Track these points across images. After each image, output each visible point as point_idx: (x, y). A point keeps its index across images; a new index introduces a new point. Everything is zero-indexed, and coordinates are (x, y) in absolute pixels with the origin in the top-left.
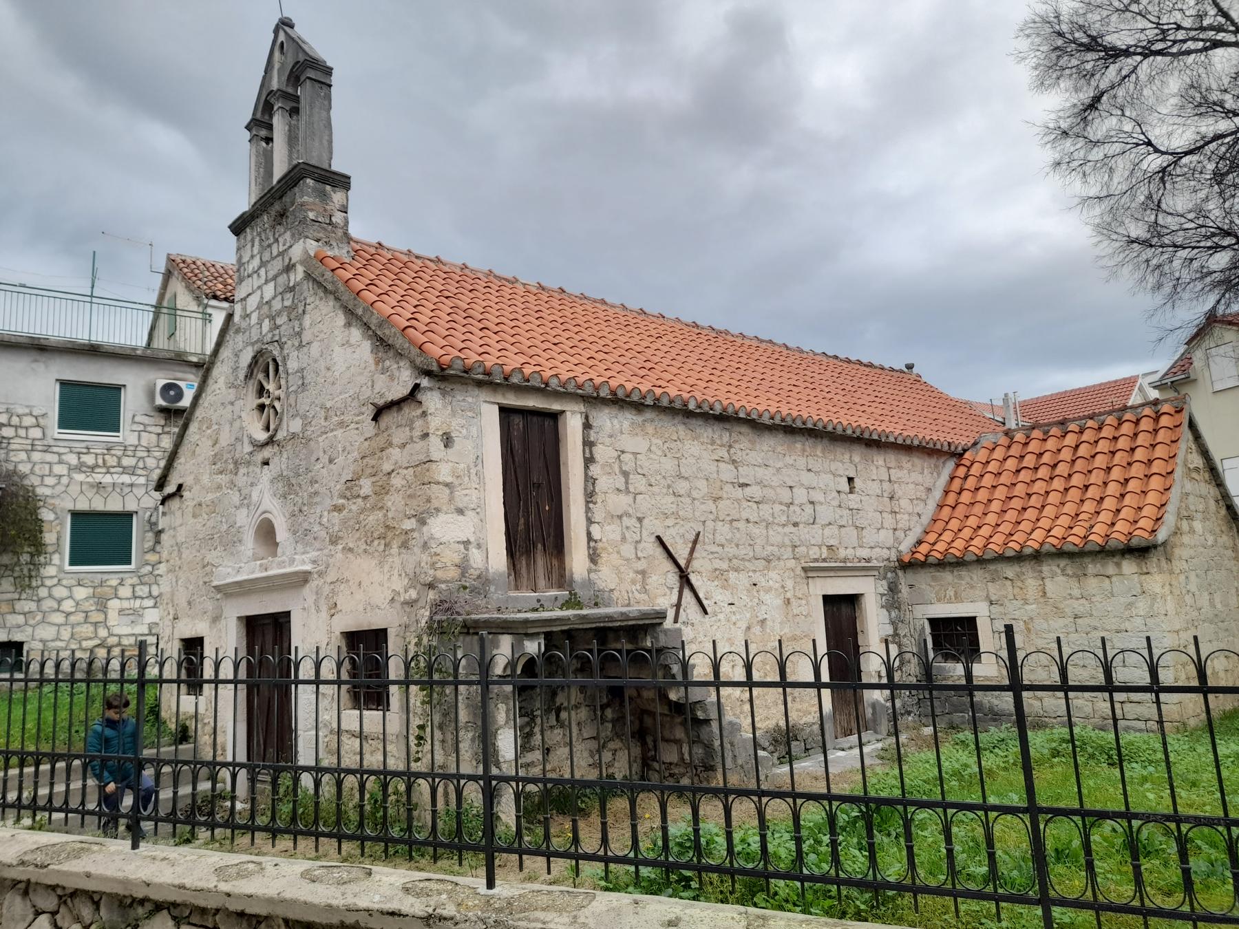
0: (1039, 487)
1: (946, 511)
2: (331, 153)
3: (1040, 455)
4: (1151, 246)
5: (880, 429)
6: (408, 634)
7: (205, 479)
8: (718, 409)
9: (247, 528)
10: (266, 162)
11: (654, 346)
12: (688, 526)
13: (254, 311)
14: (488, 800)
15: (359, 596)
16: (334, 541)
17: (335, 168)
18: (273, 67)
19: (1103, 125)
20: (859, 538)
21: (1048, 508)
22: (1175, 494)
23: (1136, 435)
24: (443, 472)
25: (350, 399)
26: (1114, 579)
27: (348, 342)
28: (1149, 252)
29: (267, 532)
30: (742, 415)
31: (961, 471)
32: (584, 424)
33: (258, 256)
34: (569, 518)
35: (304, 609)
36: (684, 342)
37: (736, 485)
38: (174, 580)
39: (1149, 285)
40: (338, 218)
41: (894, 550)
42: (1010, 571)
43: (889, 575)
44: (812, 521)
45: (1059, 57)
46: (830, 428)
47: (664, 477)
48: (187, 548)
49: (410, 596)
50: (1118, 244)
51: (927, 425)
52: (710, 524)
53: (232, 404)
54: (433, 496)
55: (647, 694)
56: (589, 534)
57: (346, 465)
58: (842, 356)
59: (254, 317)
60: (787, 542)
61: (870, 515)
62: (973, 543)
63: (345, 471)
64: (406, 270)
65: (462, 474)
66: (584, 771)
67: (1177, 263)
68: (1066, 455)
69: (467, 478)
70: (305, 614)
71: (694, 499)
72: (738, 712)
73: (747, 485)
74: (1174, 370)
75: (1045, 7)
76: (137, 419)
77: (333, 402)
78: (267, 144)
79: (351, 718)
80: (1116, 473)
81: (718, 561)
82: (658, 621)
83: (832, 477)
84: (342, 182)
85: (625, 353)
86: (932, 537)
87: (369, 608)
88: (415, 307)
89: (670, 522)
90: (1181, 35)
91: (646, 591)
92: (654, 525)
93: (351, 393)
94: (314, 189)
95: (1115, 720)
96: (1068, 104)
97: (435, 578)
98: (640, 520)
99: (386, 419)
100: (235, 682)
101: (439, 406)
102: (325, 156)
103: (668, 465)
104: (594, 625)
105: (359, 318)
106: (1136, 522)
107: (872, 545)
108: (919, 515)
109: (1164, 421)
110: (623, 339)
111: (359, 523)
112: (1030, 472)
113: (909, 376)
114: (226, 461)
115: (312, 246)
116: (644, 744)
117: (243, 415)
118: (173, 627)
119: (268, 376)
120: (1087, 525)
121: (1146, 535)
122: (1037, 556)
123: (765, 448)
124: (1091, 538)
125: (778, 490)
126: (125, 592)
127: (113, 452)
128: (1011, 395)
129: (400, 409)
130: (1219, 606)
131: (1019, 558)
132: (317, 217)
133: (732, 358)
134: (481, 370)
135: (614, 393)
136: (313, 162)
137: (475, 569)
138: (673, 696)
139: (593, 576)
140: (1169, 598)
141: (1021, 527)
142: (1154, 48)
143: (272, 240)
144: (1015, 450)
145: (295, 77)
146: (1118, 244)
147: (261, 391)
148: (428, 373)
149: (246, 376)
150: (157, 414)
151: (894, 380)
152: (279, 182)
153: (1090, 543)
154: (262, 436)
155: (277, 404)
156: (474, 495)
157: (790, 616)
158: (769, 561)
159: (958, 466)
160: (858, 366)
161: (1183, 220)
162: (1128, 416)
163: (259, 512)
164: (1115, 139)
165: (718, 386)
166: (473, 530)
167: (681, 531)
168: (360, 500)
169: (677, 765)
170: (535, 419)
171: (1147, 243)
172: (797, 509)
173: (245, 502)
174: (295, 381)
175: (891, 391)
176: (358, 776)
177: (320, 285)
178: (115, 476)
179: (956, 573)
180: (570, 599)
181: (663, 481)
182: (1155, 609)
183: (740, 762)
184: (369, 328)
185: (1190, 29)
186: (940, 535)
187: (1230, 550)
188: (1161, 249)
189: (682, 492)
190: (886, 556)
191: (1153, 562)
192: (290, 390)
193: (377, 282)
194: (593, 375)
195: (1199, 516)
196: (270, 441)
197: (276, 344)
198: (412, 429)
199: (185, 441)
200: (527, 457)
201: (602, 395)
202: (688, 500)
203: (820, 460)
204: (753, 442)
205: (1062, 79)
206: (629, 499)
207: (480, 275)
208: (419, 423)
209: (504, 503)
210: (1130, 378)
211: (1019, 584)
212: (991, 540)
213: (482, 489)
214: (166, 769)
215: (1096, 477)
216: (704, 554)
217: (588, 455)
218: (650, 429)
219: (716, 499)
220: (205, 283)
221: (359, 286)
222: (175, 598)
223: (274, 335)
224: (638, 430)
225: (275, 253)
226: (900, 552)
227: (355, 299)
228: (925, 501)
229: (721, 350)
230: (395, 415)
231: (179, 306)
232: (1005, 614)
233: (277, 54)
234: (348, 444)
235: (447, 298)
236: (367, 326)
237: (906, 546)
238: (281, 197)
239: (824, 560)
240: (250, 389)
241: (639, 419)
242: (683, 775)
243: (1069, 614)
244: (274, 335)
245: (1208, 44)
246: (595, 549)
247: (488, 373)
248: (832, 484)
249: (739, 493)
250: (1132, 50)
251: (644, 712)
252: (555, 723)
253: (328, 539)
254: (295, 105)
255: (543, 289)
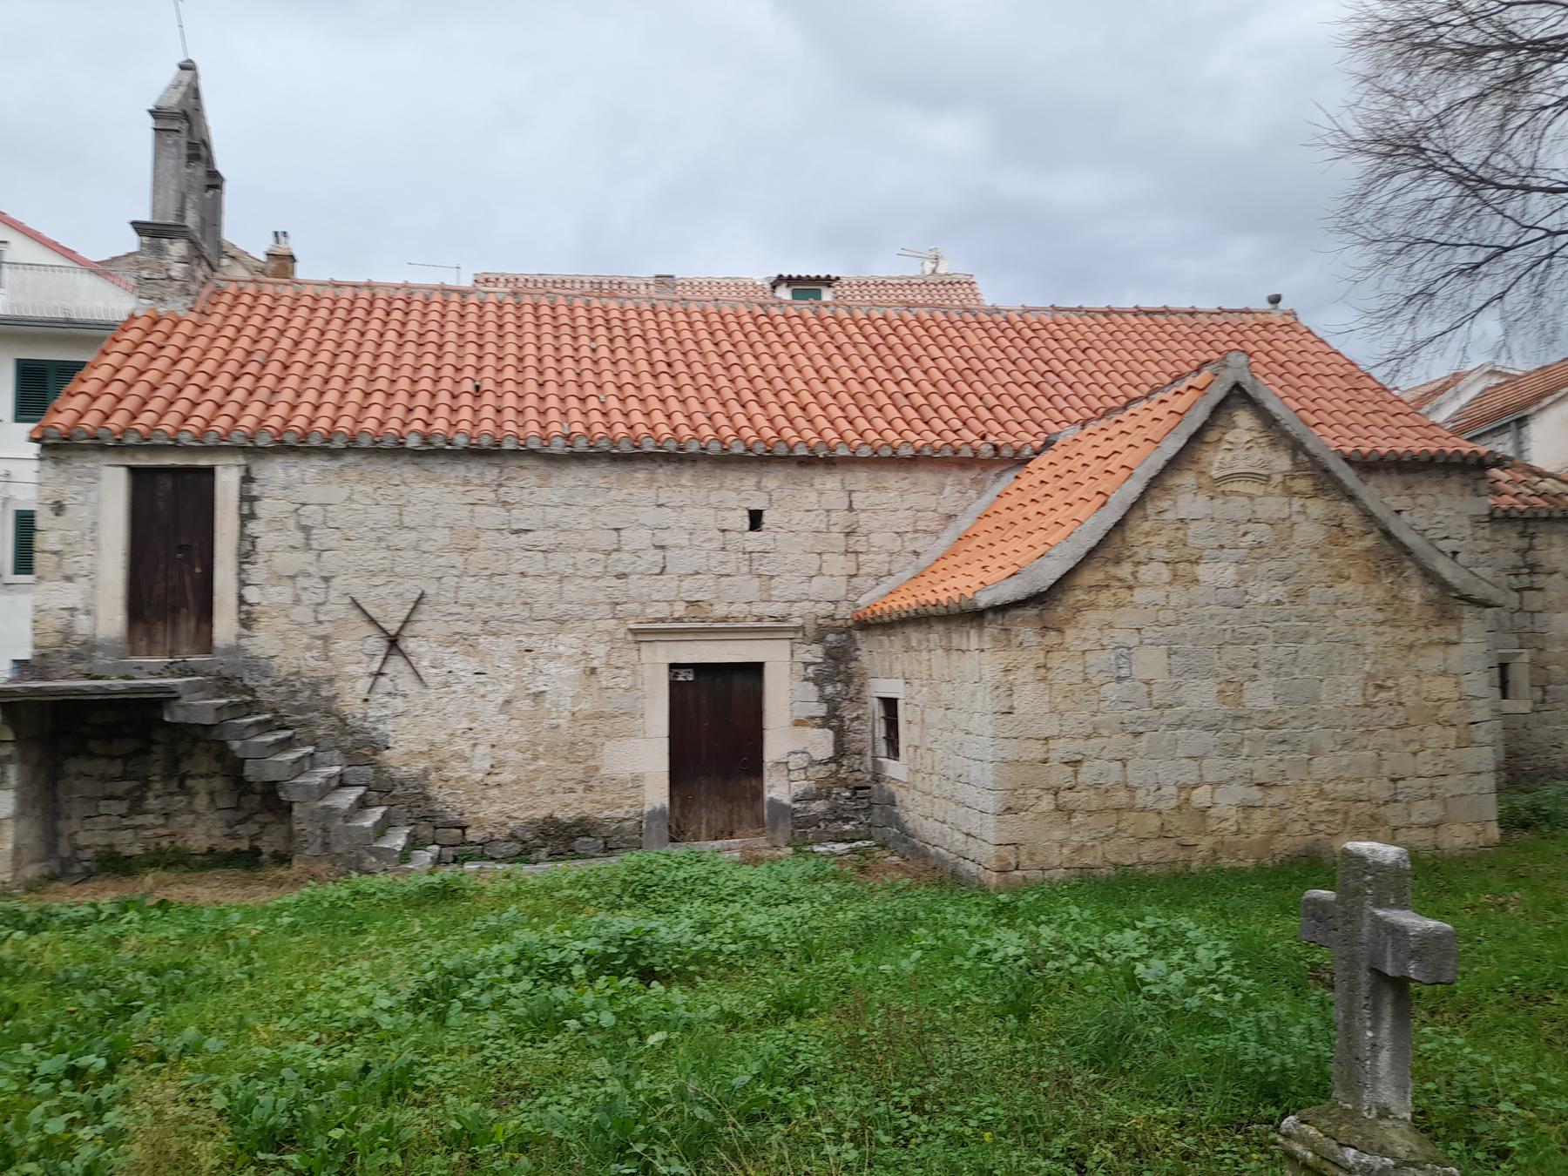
12: (409, 584)
103: (383, 515)
139: (244, 642)
218: (352, 475)
246: (248, 613)
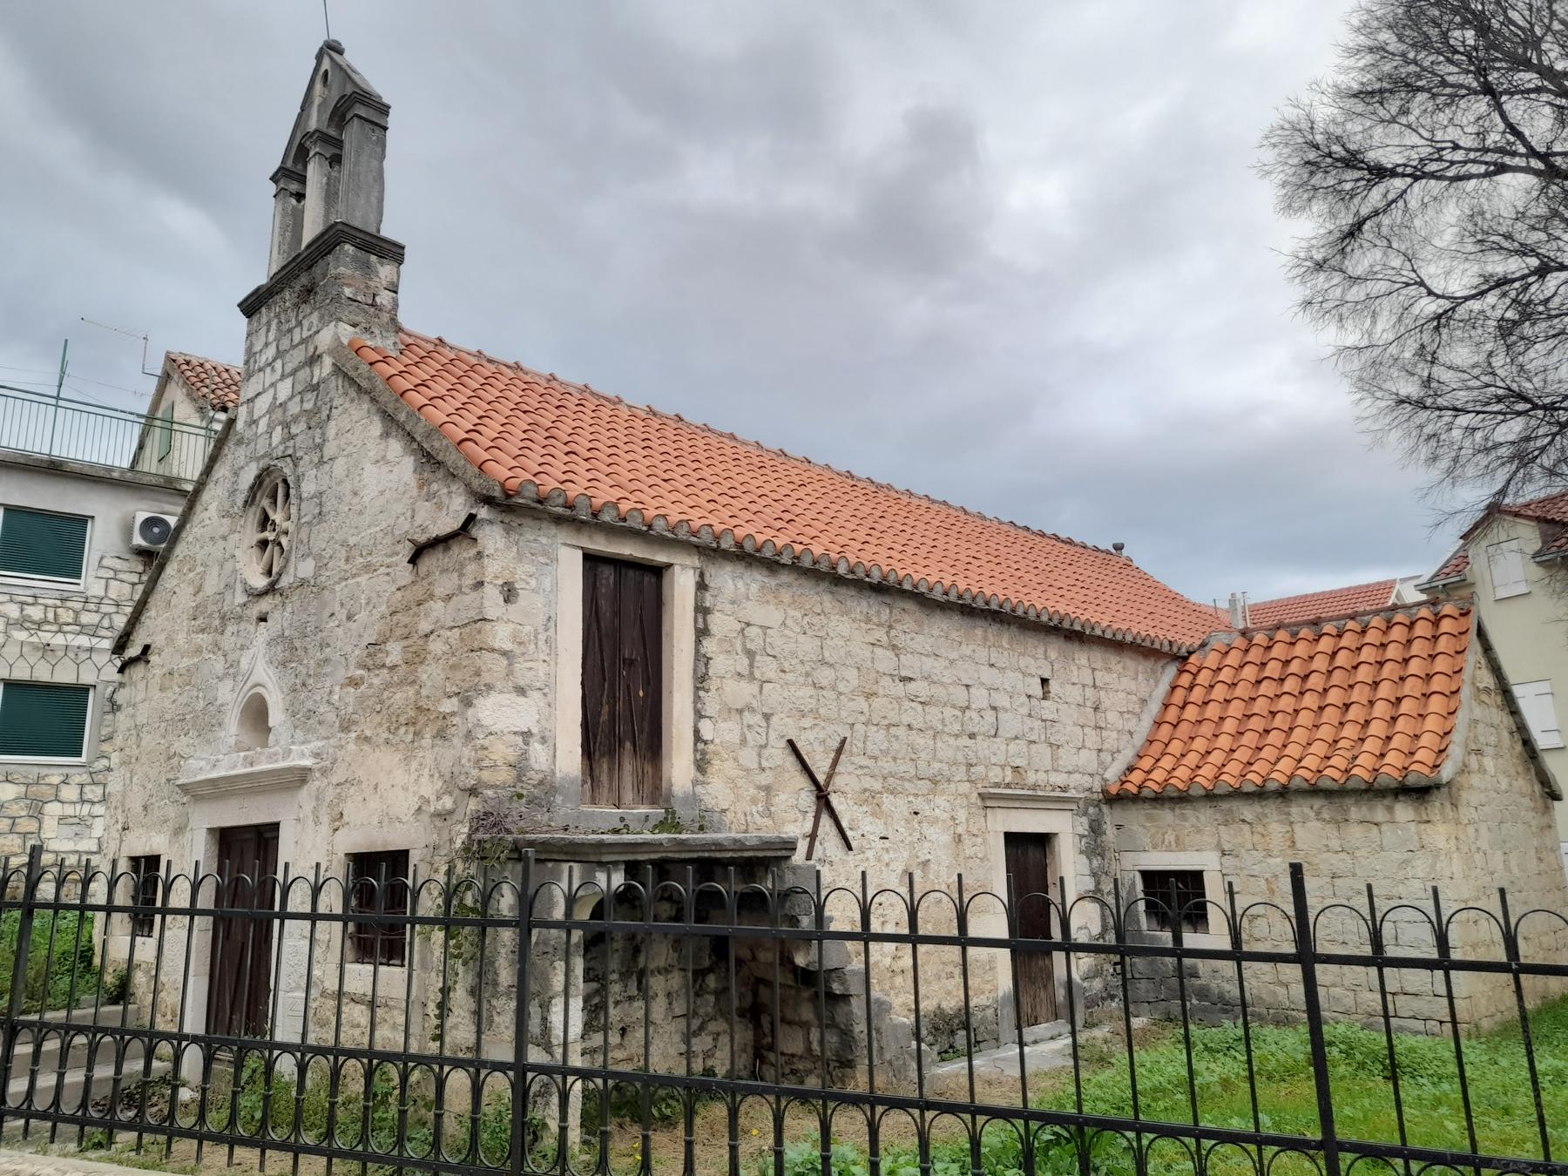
0: (1286, 703)
1: (1165, 730)
2: (381, 215)
3: (1287, 663)
4: (1426, 408)
5: (1083, 618)
6: (437, 858)
7: (181, 639)
8: (876, 577)
9: (231, 705)
10: (295, 224)
11: (795, 495)
12: (830, 729)
13: (264, 415)
14: (520, 1098)
15: (374, 803)
16: (345, 728)
17: (385, 233)
18: (312, 103)
19: (1363, 259)
20: (1054, 758)
21: (1297, 731)
22: (1461, 718)
23: (1410, 642)
24: (501, 636)
25: (381, 534)
26: (1384, 828)
27: (384, 457)
28: (1424, 415)
29: (256, 713)
30: (907, 586)
31: (1185, 680)
32: (697, 583)
33: (274, 344)
34: (671, 708)
35: (298, 820)
36: (835, 494)
37: (896, 679)
38: (128, 775)
39: (1423, 457)
40: (384, 298)
41: (1097, 778)
42: (1248, 811)
43: (1091, 810)
44: (993, 732)
45: (1312, 173)
46: (1020, 612)
47: (802, 662)
48: (148, 732)
49: (444, 806)
50: (1383, 404)
51: (1141, 619)
52: (859, 727)
53: (224, 538)
54: (483, 668)
55: (764, 956)
56: (697, 732)
57: (369, 623)
58: (1035, 528)
59: (263, 424)
60: (960, 758)
61: (1068, 730)
62: (1200, 772)
63: (369, 631)
64: (471, 374)
65: (526, 639)
66: (665, 1058)
67: (1457, 434)
68: (1320, 663)
69: (533, 646)
70: (299, 827)
71: (840, 694)
72: (887, 987)
73: (911, 679)
74: (1446, 570)
75: (1296, 111)
76: (105, 562)
77: (358, 538)
78: (299, 201)
79: (359, 976)
80: (1385, 690)
81: (868, 778)
82: (784, 853)
83: (1021, 676)
84: (393, 252)
85: (758, 500)
86: (1146, 763)
87: (386, 819)
88: (480, 418)
89: (807, 722)
90: (1459, 156)
91: (770, 815)
92: (786, 726)
93: (384, 525)
94: (355, 259)
95: (1386, 1016)
96: (1322, 231)
97: (479, 780)
98: (767, 717)
99: (428, 562)
100: (192, 912)
101: (500, 545)
102: (372, 218)
103: (808, 646)
104: (695, 855)
105: (400, 426)
106: (1412, 754)
107: (1071, 769)
108: (1131, 734)
109: (1446, 625)
110: (756, 483)
111: (382, 702)
112: (1274, 683)
113: (1117, 559)
114: (210, 616)
115: (346, 332)
116: (757, 1026)
117: (238, 553)
118: (122, 841)
119: (275, 502)
120: (1349, 755)
121: (1426, 771)
122: (1284, 793)
123: (936, 632)
124: (1354, 771)
125: (951, 689)
126: (69, 793)
127: (69, 604)
128: (1239, 596)
129: (447, 549)
130: (1516, 870)
131: (1260, 794)
132: (355, 294)
133: (895, 518)
134: (561, 501)
135: (739, 545)
136: (357, 223)
137: (537, 772)
138: (800, 960)
139: (699, 789)
140: (1455, 855)
141: (1263, 754)
142: (1426, 169)
143: (294, 322)
144: (1255, 654)
145: (340, 115)
146: (1383, 404)
147: (265, 522)
148: (488, 500)
149: (246, 502)
150: (134, 557)
151: (1098, 562)
152: (308, 247)
153: (1354, 779)
154: (261, 582)
155: (284, 541)
156: (542, 669)
157: (961, 859)
158: (936, 783)
159: (1181, 672)
160: (1054, 542)
161: (1466, 376)
162: (1399, 617)
163: (249, 684)
164: (1380, 276)
165: (876, 549)
166: (537, 717)
167: (821, 735)
168: (385, 671)
169: (801, 1057)
170: (631, 573)
171: (1420, 404)
172: (975, 715)
173: (232, 665)
174: (310, 509)
175: (1095, 575)
176: (331, 1058)
177: (352, 381)
178: (69, 637)
179: (1178, 811)
180: (666, 819)
181: (799, 667)
182: (1438, 869)
183: (888, 1056)
184: (413, 439)
185: (1470, 150)
186: (1158, 760)
187: (1528, 799)
188: (1437, 413)
189: (825, 683)
190: (1087, 786)
191: (1436, 805)
192: (303, 520)
193: (430, 383)
194: (712, 520)
195: (1489, 750)
196: (271, 589)
197: (288, 459)
198: (461, 575)
199: (159, 587)
200: (617, 623)
201: (724, 546)
202: (831, 695)
203: (1006, 653)
204: (919, 624)
205: (1314, 202)
206: (754, 688)
207: (571, 390)
208: (471, 568)
209: (583, 683)
210: (1385, 583)
211: (1260, 829)
212: (1225, 770)
213: (552, 663)
214: (80, 1040)
215: (1359, 694)
216: (851, 768)
217: (701, 625)
218: (786, 596)
219: (870, 695)
220: (213, 391)
221: (403, 384)
222: (127, 801)
223: (287, 447)
224: (770, 597)
225: (297, 339)
226: (1105, 780)
227: (397, 400)
228: (1138, 716)
229: (881, 508)
230: (441, 556)
231: (175, 419)
232: (1241, 869)
233: (318, 86)
234: (374, 595)
235: (525, 412)
236: (410, 437)
237: (1113, 773)
238: (310, 268)
239: (1008, 786)
240: (250, 520)
241: (772, 582)
242: (809, 1072)
243: (1326, 872)
244: (287, 447)
245: (1492, 168)
246: (704, 753)
247: (570, 506)
248: (1020, 685)
249: (899, 689)
250: (1400, 170)
251: (760, 981)
252: (636, 993)
253: (337, 724)
254: (337, 151)
255: (655, 415)
